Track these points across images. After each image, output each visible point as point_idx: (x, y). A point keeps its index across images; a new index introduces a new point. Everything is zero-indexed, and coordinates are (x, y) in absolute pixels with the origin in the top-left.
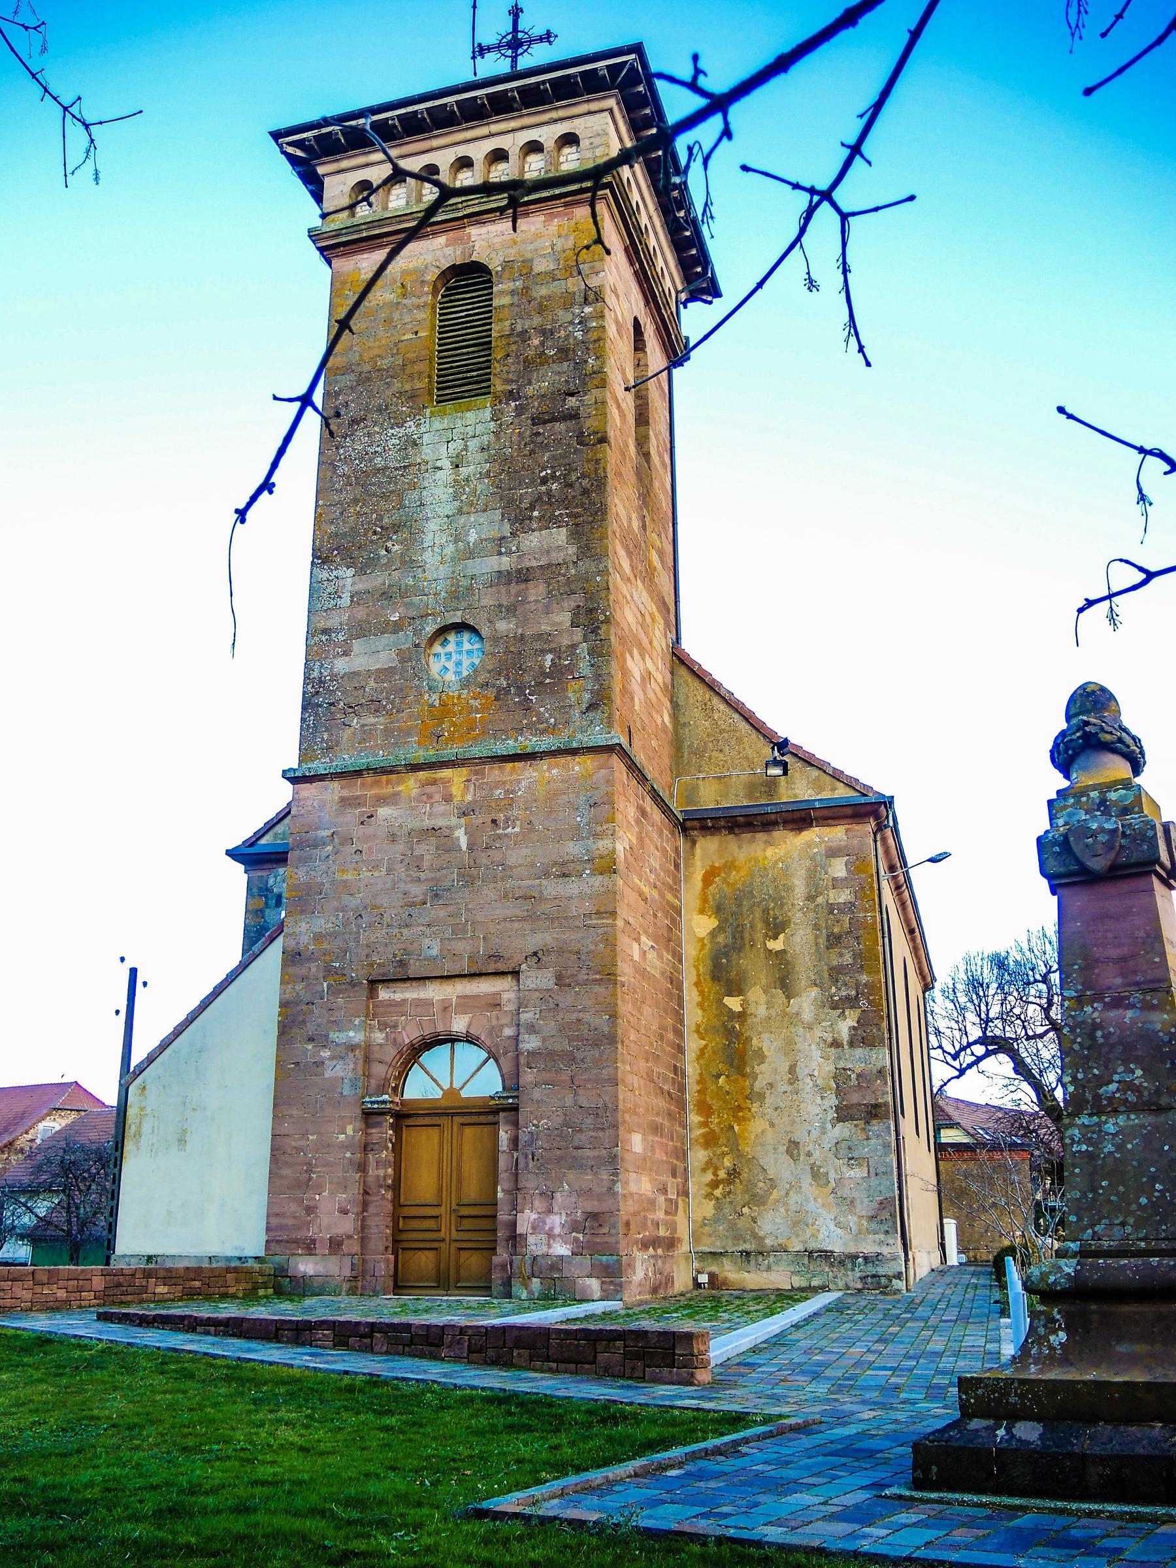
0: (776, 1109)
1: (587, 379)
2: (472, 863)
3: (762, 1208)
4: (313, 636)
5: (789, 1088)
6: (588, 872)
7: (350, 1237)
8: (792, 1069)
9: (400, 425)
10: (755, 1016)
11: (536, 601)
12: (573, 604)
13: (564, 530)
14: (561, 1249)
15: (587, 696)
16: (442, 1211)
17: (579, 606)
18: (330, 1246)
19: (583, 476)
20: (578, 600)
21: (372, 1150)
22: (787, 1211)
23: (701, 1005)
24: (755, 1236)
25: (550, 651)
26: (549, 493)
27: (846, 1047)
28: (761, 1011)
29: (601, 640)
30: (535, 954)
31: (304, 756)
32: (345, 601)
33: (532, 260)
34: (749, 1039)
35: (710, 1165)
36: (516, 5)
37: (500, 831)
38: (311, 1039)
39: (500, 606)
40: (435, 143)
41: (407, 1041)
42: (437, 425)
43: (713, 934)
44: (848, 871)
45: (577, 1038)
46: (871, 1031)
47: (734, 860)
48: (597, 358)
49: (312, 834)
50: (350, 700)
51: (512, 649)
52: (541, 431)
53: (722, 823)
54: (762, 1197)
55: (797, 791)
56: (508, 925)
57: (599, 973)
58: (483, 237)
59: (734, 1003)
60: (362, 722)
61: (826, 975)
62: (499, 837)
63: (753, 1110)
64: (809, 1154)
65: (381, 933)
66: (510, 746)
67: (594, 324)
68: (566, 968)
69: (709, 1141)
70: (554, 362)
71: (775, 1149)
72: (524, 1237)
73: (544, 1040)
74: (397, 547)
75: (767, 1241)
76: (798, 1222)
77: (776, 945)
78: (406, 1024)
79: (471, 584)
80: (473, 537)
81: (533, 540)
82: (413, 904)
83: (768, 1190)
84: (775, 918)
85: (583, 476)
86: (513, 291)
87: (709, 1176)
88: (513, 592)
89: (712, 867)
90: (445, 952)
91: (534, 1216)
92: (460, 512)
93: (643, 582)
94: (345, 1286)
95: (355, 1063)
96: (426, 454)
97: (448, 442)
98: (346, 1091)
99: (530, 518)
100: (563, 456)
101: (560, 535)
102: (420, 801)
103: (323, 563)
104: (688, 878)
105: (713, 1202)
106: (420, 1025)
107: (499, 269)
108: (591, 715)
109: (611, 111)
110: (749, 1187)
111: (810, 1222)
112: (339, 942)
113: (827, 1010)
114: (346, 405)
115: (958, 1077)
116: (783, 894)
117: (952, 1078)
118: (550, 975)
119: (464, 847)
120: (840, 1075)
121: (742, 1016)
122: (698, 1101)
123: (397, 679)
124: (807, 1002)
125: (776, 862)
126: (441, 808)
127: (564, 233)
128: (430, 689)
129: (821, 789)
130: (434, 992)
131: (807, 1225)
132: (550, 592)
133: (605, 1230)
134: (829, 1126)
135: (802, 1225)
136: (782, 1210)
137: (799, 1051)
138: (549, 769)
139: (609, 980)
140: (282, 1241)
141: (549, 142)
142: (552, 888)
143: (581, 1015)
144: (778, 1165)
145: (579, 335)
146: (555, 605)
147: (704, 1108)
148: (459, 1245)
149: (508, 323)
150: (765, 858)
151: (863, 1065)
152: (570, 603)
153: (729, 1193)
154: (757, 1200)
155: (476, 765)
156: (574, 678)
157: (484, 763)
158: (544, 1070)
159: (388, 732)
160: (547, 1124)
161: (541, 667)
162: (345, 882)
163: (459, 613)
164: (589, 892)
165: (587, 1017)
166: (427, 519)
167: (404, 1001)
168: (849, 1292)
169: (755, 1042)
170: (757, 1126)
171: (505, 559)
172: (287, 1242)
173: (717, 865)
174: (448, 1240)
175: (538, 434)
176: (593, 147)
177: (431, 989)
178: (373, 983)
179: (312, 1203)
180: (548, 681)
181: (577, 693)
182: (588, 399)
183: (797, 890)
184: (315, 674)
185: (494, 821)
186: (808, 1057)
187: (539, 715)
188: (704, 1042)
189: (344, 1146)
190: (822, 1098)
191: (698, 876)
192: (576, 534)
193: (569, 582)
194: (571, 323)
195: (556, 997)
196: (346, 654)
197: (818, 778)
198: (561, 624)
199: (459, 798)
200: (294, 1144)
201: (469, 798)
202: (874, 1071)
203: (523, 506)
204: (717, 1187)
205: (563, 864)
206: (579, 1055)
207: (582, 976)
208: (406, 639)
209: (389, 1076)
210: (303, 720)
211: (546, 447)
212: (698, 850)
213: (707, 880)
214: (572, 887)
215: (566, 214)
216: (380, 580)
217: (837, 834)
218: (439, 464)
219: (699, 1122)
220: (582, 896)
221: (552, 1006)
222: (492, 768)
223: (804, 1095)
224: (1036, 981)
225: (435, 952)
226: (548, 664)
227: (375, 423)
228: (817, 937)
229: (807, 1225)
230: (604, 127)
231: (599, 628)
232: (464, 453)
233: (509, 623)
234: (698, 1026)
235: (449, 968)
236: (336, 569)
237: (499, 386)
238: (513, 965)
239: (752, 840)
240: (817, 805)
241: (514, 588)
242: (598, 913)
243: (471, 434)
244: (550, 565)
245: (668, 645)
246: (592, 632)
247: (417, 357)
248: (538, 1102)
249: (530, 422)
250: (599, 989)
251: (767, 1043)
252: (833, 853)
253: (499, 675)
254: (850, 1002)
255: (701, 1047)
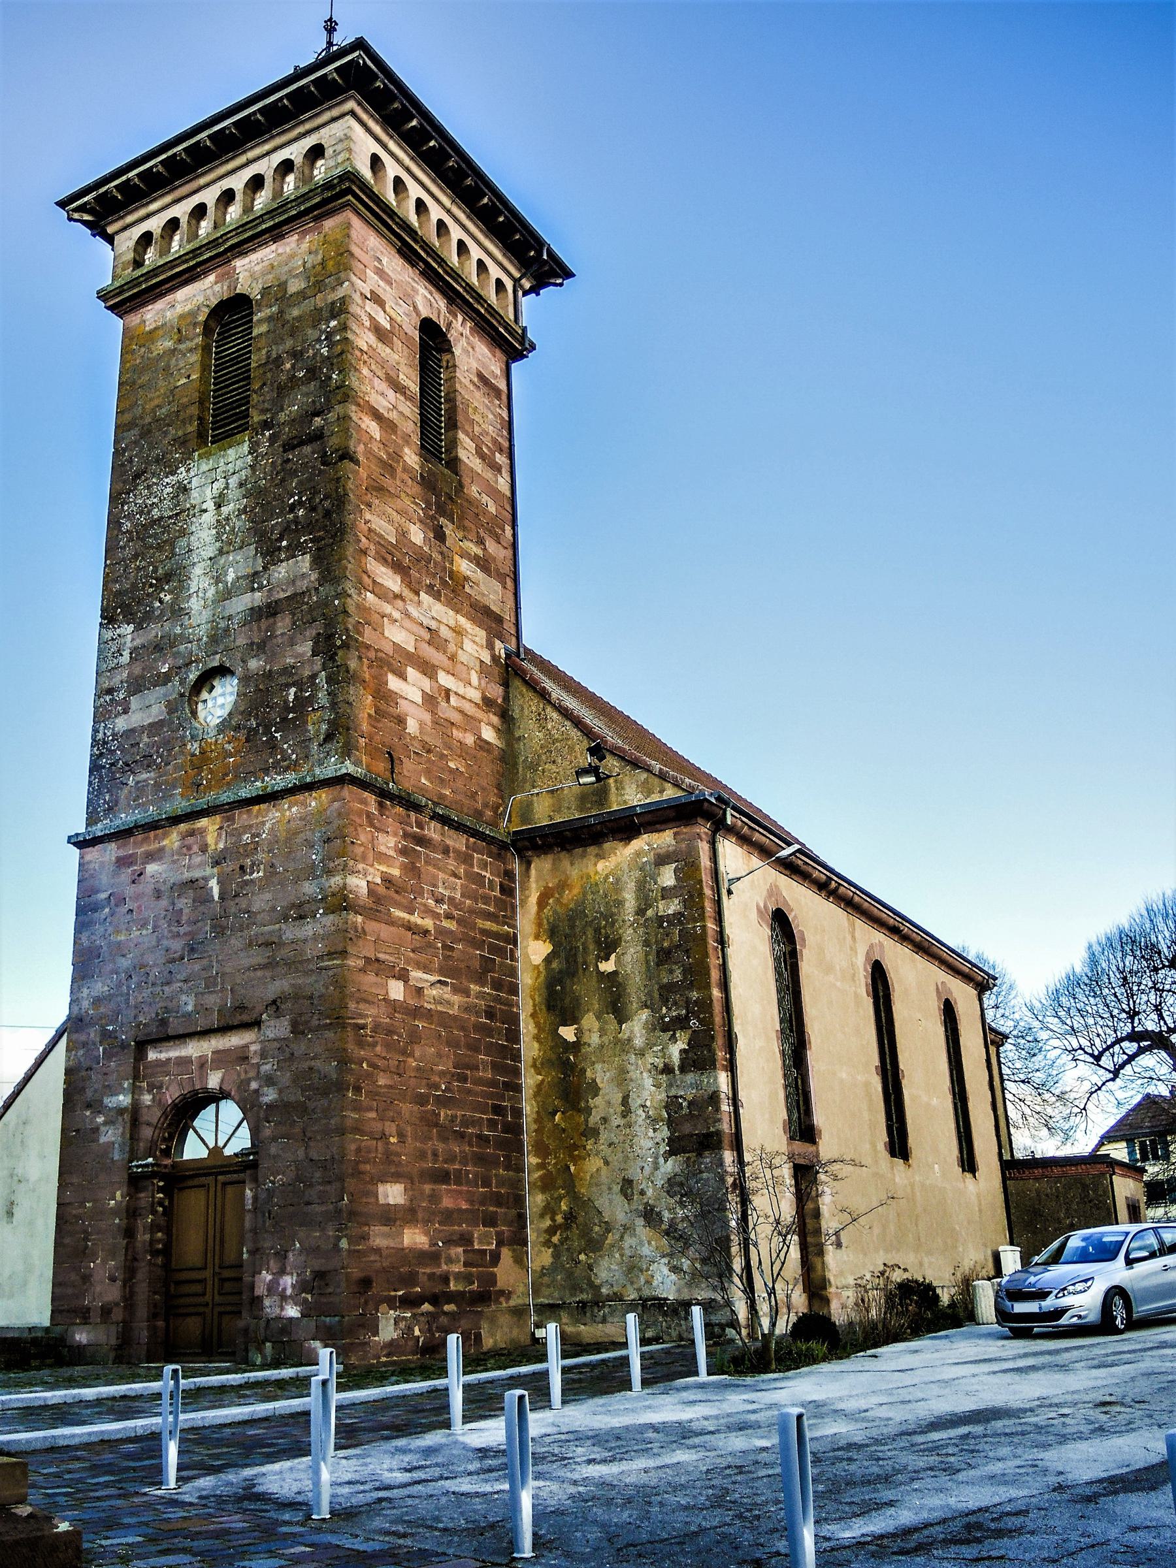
0: (610, 1145)
1: (331, 396)
2: (223, 913)
3: (598, 1254)
4: (99, 698)
5: (621, 1122)
6: (321, 911)
7: (117, 1304)
8: (625, 1101)
9: (173, 473)
10: (589, 1045)
11: (282, 634)
12: (314, 632)
13: (308, 556)
14: (292, 1312)
15: (324, 727)
16: (208, 1274)
17: (319, 634)
18: (102, 1314)
19: (326, 497)
20: (318, 628)
21: (140, 1215)
22: (622, 1255)
23: (537, 1038)
24: (591, 1284)
25: (293, 685)
26: (296, 521)
27: (677, 1072)
28: (594, 1039)
29: (337, 667)
30: (274, 1002)
31: (91, 820)
32: (126, 658)
33: (286, 282)
34: (583, 1071)
35: (549, 1210)
36: (331, 18)
37: (247, 877)
38: (89, 1106)
39: (252, 644)
40: (202, 181)
41: (170, 1101)
42: (205, 467)
43: (548, 960)
44: (677, 878)
45: (309, 1088)
46: (702, 1052)
47: (567, 878)
48: (340, 372)
49: (94, 898)
50: (128, 758)
51: (261, 687)
52: (291, 457)
53: (550, 840)
54: (598, 1242)
55: (627, 797)
56: (252, 974)
57: (328, 1017)
58: (246, 267)
59: (568, 1033)
60: (137, 779)
61: (656, 995)
62: (246, 883)
63: (588, 1147)
64: (642, 1193)
65: (146, 993)
66: (256, 787)
67: (338, 338)
68: (301, 1015)
69: (546, 1185)
70: (303, 384)
71: (610, 1189)
72: (260, 1299)
73: (280, 1091)
74: (168, 597)
75: (604, 1290)
76: (633, 1267)
77: (607, 966)
78: (169, 1084)
79: (228, 625)
80: (231, 576)
81: (281, 572)
82: (173, 961)
83: (603, 1235)
84: (607, 937)
85: (326, 497)
86: (270, 317)
87: (548, 1223)
88: (263, 627)
89: (546, 888)
90: (199, 1007)
91: (269, 1277)
92: (221, 552)
93: (437, 596)
94: (112, 1355)
95: (124, 1128)
96: (194, 498)
97: (213, 483)
98: (117, 1157)
99: (280, 549)
100: (310, 480)
101: (304, 562)
102: (180, 854)
103: (109, 623)
104: (523, 902)
105: (551, 1250)
106: (180, 1084)
107: (259, 297)
108: (328, 746)
109: (352, 113)
110: (586, 1233)
111: (645, 1267)
112: (112, 1005)
113: (658, 1033)
114: (130, 461)
115: (1113, 1080)
116: (615, 910)
117: (1107, 1081)
118: (286, 1023)
119: (216, 898)
120: (672, 1104)
121: (576, 1046)
122: (536, 1141)
123: (167, 733)
124: (637, 1027)
125: (607, 876)
126: (197, 860)
127: (314, 248)
128: (192, 738)
129: (649, 792)
130: (193, 1049)
131: (641, 1271)
132: (294, 623)
133: (330, 1290)
134: (661, 1160)
135: (636, 1271)
136: (617, 1255)
137: (632, 1080)
138: (290, 808)
139: (338, 1024)
140: (63, 1311)
141: (298, 160)
142: (291, 932)
143: (313, 1063)
144: (615, 1209)
145: (325, 351)
146: (299, 635)
147: (541, 1149)
148: (222, 1309)
149: (264, 352)
150: (596, 873)
151: (694, 1091)
152: (311, 632)
153: (567, 1238)
154: (594, 1245)
155: (226, 811)
156: (314, 709)
157: (231, 809)
158: (280, 1123)
159: (157, 785)
160: (282, 1180)
161: (286, 702)
162: (119, 943)
163: (218, 656)
164: (322, 932)
165: (317, 1064)
166: (194, 564)
167: (169, 1060)
168: (683, 1343)
169: (589, 1074)
170: (593, 1164)
171: (258, 595)
172: (68, 1311)
173: (550, 885)
174: (210, 1303)
175: (288, 460)
176: (336, 154)
177: (190, 1046)
178: (142, 1046)
179: (87, 1272)
180: (291, 716)
181: (316, 725)
182: (332, 416)
183: (627, 905)
184: (100, 736)
185: (242, 868)
186: (641, 1087)
187: (283, 751)
188: (540, 1078)
189: (115, 1212)
190: (655, 1130)
191: (533, 899)
192: (317, 562)
193: (311, 609)
194: (319, 340)
195: (292, 1046)
196: (126, 712)
197: (646, 780)
198: (302, 655)
199: (213, 847)
200: (74, 1212)
201: (221, 846)
202: (706, 1097)
203: (274, 537)
204: (555, 1234)
205: (300, 905)
206: (311, 1105)
207: (315, 1022)
208: (174, 687)
209: (155, 1138)
210: (90, 783)
211: (294, 473)
212: (533, 872)
213: (542, 903)
214: (308, 929)
215: (318, 228)
216: (153, 633)
217: (665, 839)
218: (204, 506)
219: (537, 1164)
220: (315, 939)
221: (288, 1055)
222: (240, 813)
223: (637, 1128)
224: (1164, 966)
225: (190, 1008)
226: (291, 698)
227: (154, 474)
228: (647, 954)
229: (641, 1271)
230: (346, 131)
231: (336, 654)
232: (225, 491)
233: (260, 660)
234: (535, 1060)
235: (202, 1024)
236: (119, 627)
237: (256, 417)
238: (255, 1016)
239: (583, 856)
240: (638, 810)
241: (264, 624)
242: (330, 954)
243: (232, 471)
244: (295, 595)
245: (495, 658)
246: (330, 660)
247: (189, 401)
248: (274, 1157)
249: (281, 449)
250: (329, 1034)
251: (600, 1074)
252: (662, 860)
253: (250, 715)
254: (680, 1023)
255: (538, 1082)
